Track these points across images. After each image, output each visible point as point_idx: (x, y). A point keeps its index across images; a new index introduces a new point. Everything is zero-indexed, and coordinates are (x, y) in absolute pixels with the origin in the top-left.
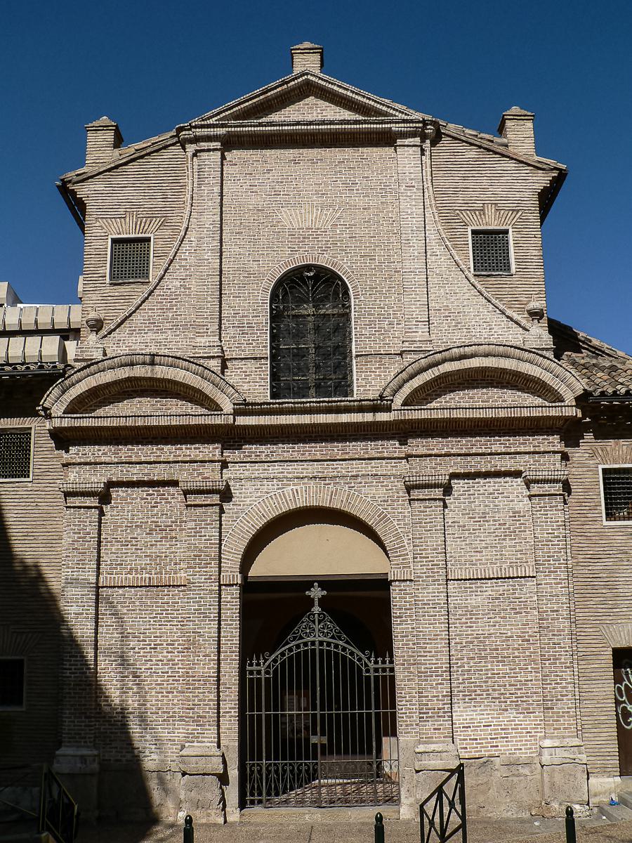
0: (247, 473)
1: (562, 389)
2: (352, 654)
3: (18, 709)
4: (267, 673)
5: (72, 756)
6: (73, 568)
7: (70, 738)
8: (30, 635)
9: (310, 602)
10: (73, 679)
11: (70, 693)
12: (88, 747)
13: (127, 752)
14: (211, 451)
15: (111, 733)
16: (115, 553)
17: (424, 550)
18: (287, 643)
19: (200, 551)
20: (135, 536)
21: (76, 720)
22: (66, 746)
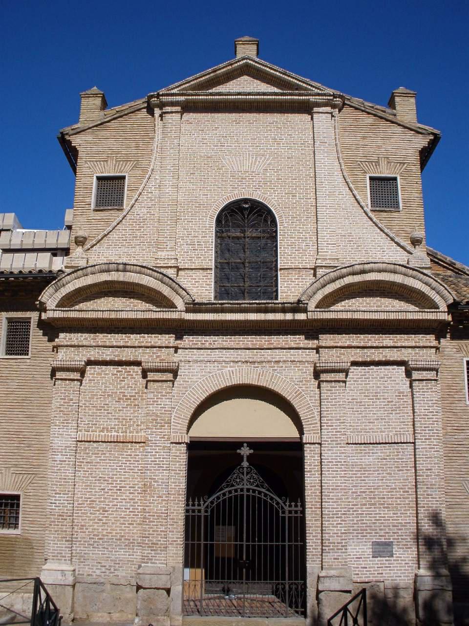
1: (437, 299)
2: (272, 499)
4: (206, 511)
9: (241, 458)
13: (97, 569)
14: (168, 339)
18: (222, 489)
19: (157, 416)
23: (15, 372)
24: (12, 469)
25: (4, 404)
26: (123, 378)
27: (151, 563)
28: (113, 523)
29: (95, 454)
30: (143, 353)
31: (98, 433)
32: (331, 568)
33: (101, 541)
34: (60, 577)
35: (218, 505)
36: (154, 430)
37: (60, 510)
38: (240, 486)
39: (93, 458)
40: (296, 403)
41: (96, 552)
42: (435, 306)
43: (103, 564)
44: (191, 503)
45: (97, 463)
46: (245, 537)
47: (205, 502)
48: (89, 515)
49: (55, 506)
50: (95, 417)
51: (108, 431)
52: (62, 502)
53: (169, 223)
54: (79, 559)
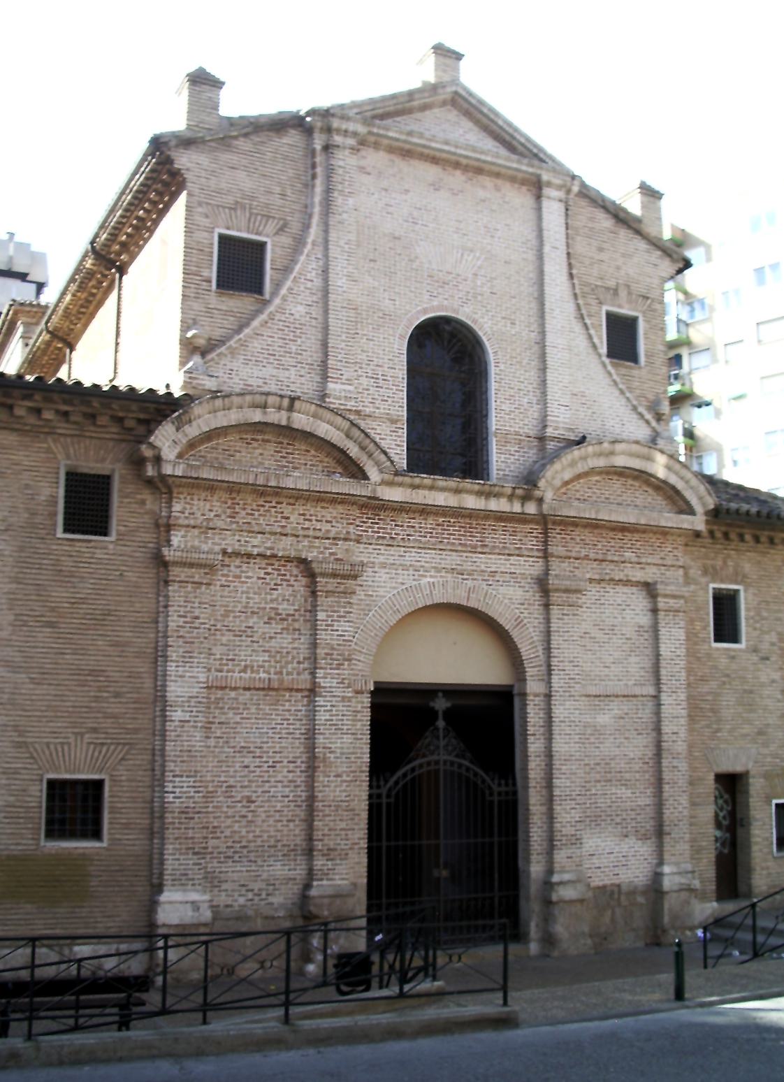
0: (381, 559)
1: (694, 502)
2: (476, 774)
3: (97, 844)
4: (388, 796)
5: (181, 903)
6: (177, 662)
7: (173, 880)
8: (112, 747)
9: (433, 714)
10: (177, 805)
11: (174, 823)
12: (197, 891)
13: (240, 895)
15: (220, 872)
16: (226, 645)
17: (562, 661)
18: (410, 762)
19: (333, 649)
20: (251, 625)
21: (182, 857)
22: (170, 891)
23: (86, 565)
24: (87, 736)
25: (68, 621)
26: (275, 585)
27: (328, 880)
28: (263, 821)
29: (233, 709)
30: (310, 547)
31: (224, 674)
32: (563, 871)
33: (245, 851)
34: (190, 913)
35: (405, 786)
36: (329, 671)
37: (182, 802)
38: (435, 757)
39: (231, 715)
40: (515, 634)
41: (238, 869)
42: (691, 512)
43: (250, 887)
44: (375, 784)
45: (238, 723)
46: (496, 829)
47: (386, 781)
48: (225, 809)
49: (174, 798)
50: (232, 648)
51: (252, 672)
52: (185, 789)
53: (344, 338)
54: (211, 882)
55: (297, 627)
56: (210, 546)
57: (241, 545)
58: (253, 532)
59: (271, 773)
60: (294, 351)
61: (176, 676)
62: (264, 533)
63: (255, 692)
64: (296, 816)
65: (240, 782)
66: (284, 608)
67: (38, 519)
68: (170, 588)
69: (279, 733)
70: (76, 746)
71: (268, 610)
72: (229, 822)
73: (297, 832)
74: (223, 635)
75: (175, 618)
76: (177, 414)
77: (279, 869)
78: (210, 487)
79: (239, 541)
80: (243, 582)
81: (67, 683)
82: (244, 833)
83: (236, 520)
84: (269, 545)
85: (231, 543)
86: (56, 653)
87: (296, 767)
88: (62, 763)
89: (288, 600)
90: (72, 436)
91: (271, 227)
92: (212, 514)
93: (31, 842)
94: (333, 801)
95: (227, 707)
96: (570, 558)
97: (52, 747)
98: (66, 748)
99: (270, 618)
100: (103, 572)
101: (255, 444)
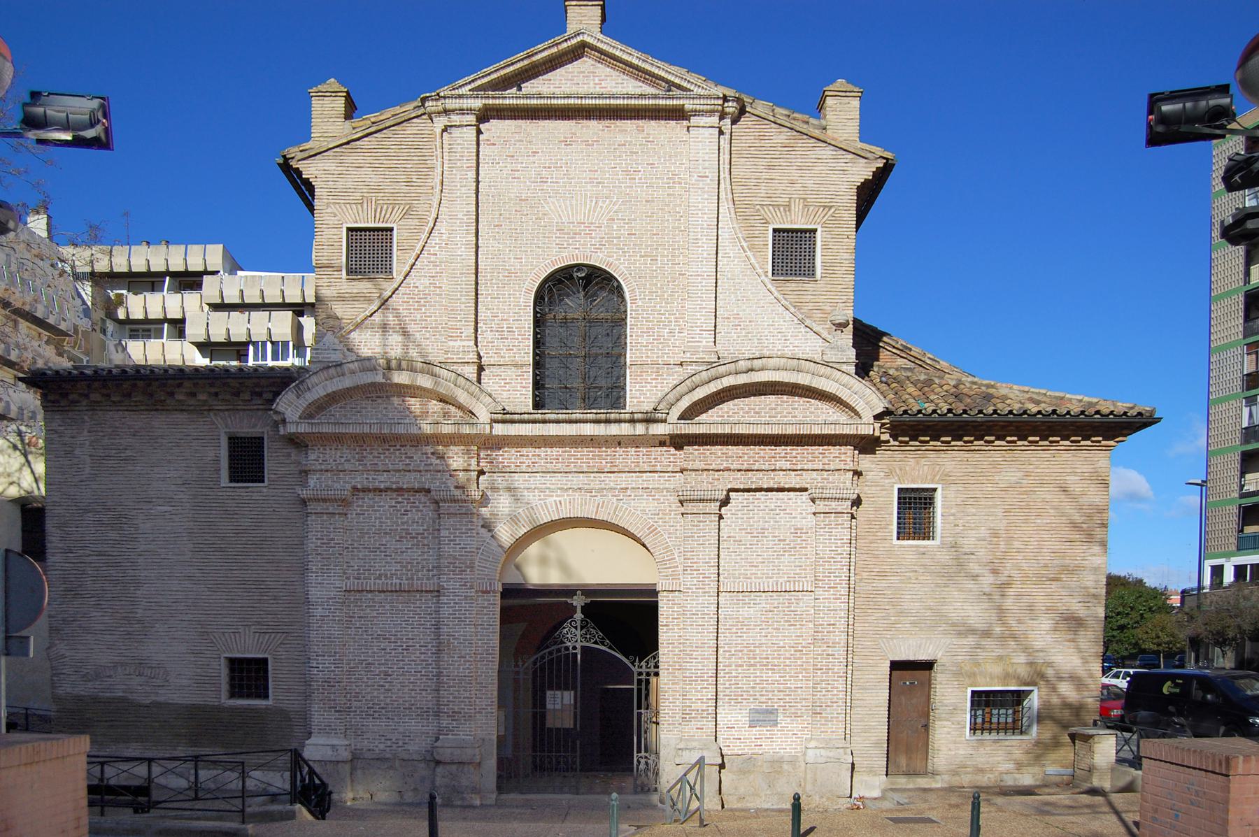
10: (321, 676)
18: (548, 647)
19: (455, 558)
20: (384, 543)
24: (253, 627)
25: (234, 546)
29: (371, 606)
30: (432, 479)
34: (330, 753)
48: (366, 680)
50: (367, 561)
52: (327, 665)
55: (426, 543)
56: (342, 485)
57: (369, 482)
58: (379, 471)
59: (405, 654)
60: (418, 318)
61: (315, 583)
62: (389, 471)
63: (389, 594)
64: (428, 686)
65: (378, 660)
66: (414, 529)
67: (206, 474)
68: (309, 518)
69: (411, 624)
70: (245, 635)
71: (399, 531)
72: (369, 689)
73: (429, 698)
74: (360, 551)
75: (314, 540)
76: (294, 384)
77: (413, 725)
78: (338, 439)
79: (367, 479)
80: (375, 511)
81: (236, 590)
82: (382, 698)
83: (365, 462)
84: (394, 479)
85: (360, 481)
86: (226, 570)
87: (428, 650)
88: (235, 646)
89: (418, 522)
90: (227, 410)
91: (397, 214)
92: (343, 460)
93: (215, 700)
94: (457, 676)
95: (365, 605)
96: (708, 470)
97: (226, 635)
98: (237, 635)
99: (401, 537)
100: (259, 509)
101: (380, 401)
